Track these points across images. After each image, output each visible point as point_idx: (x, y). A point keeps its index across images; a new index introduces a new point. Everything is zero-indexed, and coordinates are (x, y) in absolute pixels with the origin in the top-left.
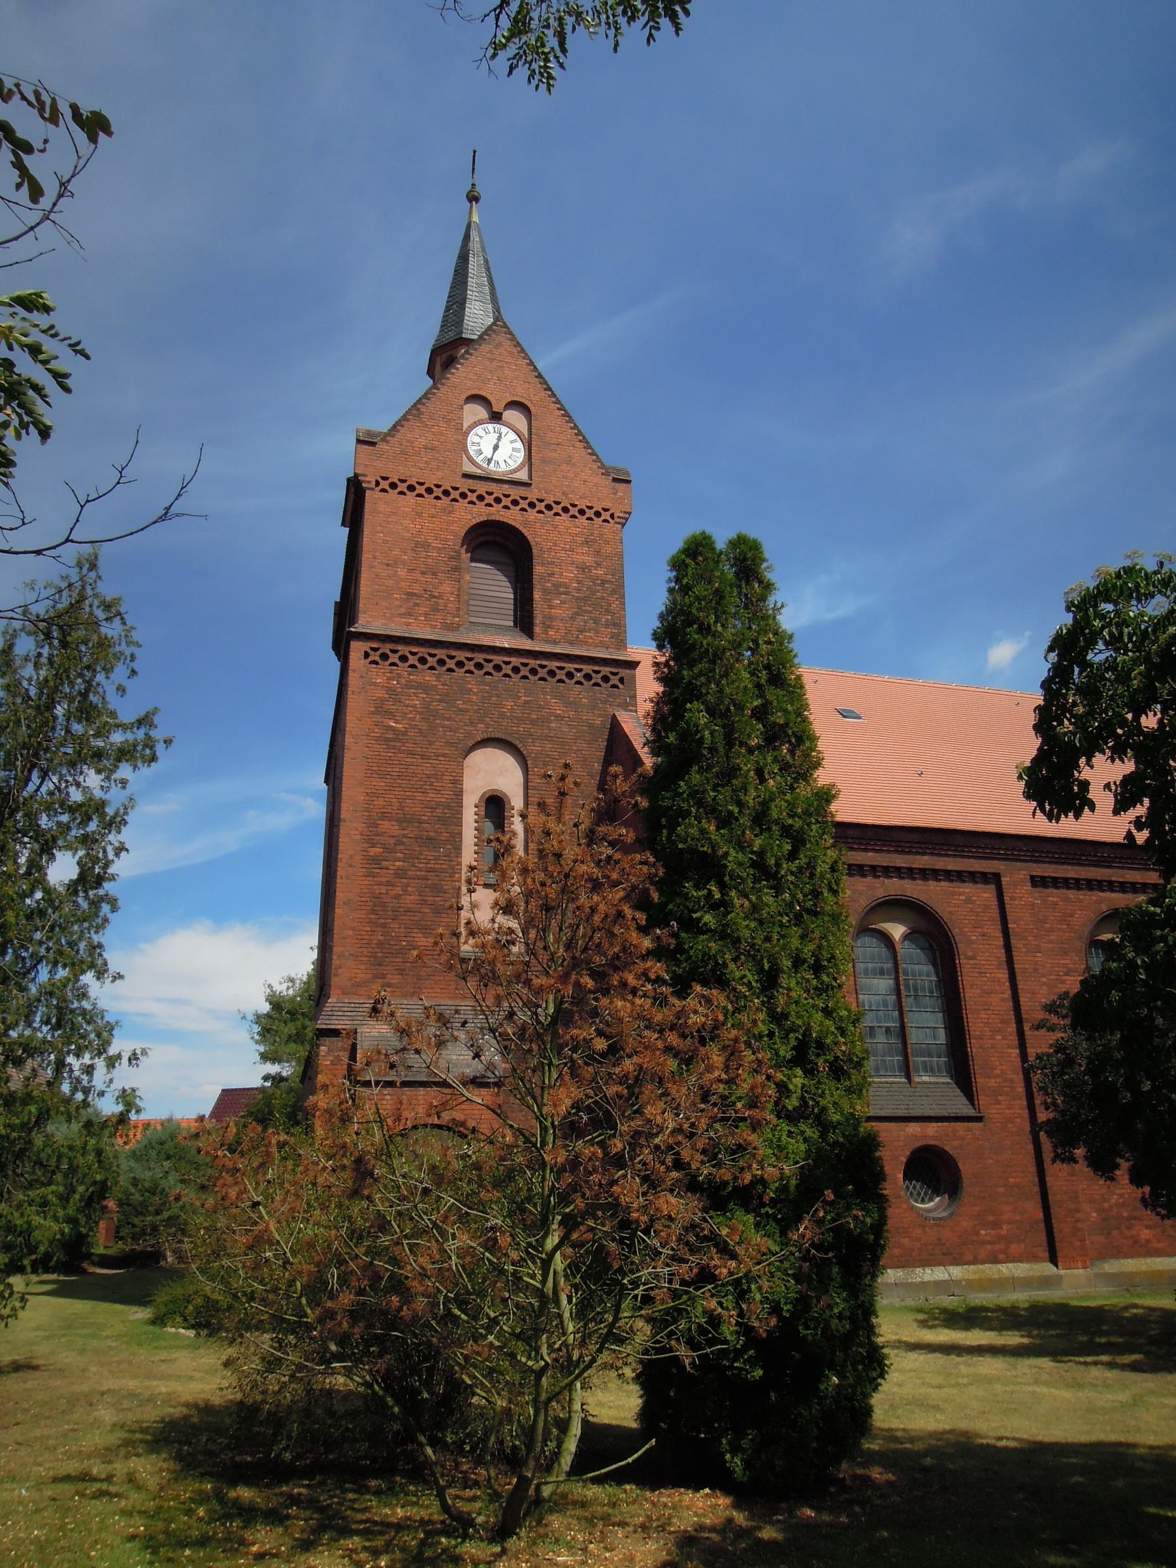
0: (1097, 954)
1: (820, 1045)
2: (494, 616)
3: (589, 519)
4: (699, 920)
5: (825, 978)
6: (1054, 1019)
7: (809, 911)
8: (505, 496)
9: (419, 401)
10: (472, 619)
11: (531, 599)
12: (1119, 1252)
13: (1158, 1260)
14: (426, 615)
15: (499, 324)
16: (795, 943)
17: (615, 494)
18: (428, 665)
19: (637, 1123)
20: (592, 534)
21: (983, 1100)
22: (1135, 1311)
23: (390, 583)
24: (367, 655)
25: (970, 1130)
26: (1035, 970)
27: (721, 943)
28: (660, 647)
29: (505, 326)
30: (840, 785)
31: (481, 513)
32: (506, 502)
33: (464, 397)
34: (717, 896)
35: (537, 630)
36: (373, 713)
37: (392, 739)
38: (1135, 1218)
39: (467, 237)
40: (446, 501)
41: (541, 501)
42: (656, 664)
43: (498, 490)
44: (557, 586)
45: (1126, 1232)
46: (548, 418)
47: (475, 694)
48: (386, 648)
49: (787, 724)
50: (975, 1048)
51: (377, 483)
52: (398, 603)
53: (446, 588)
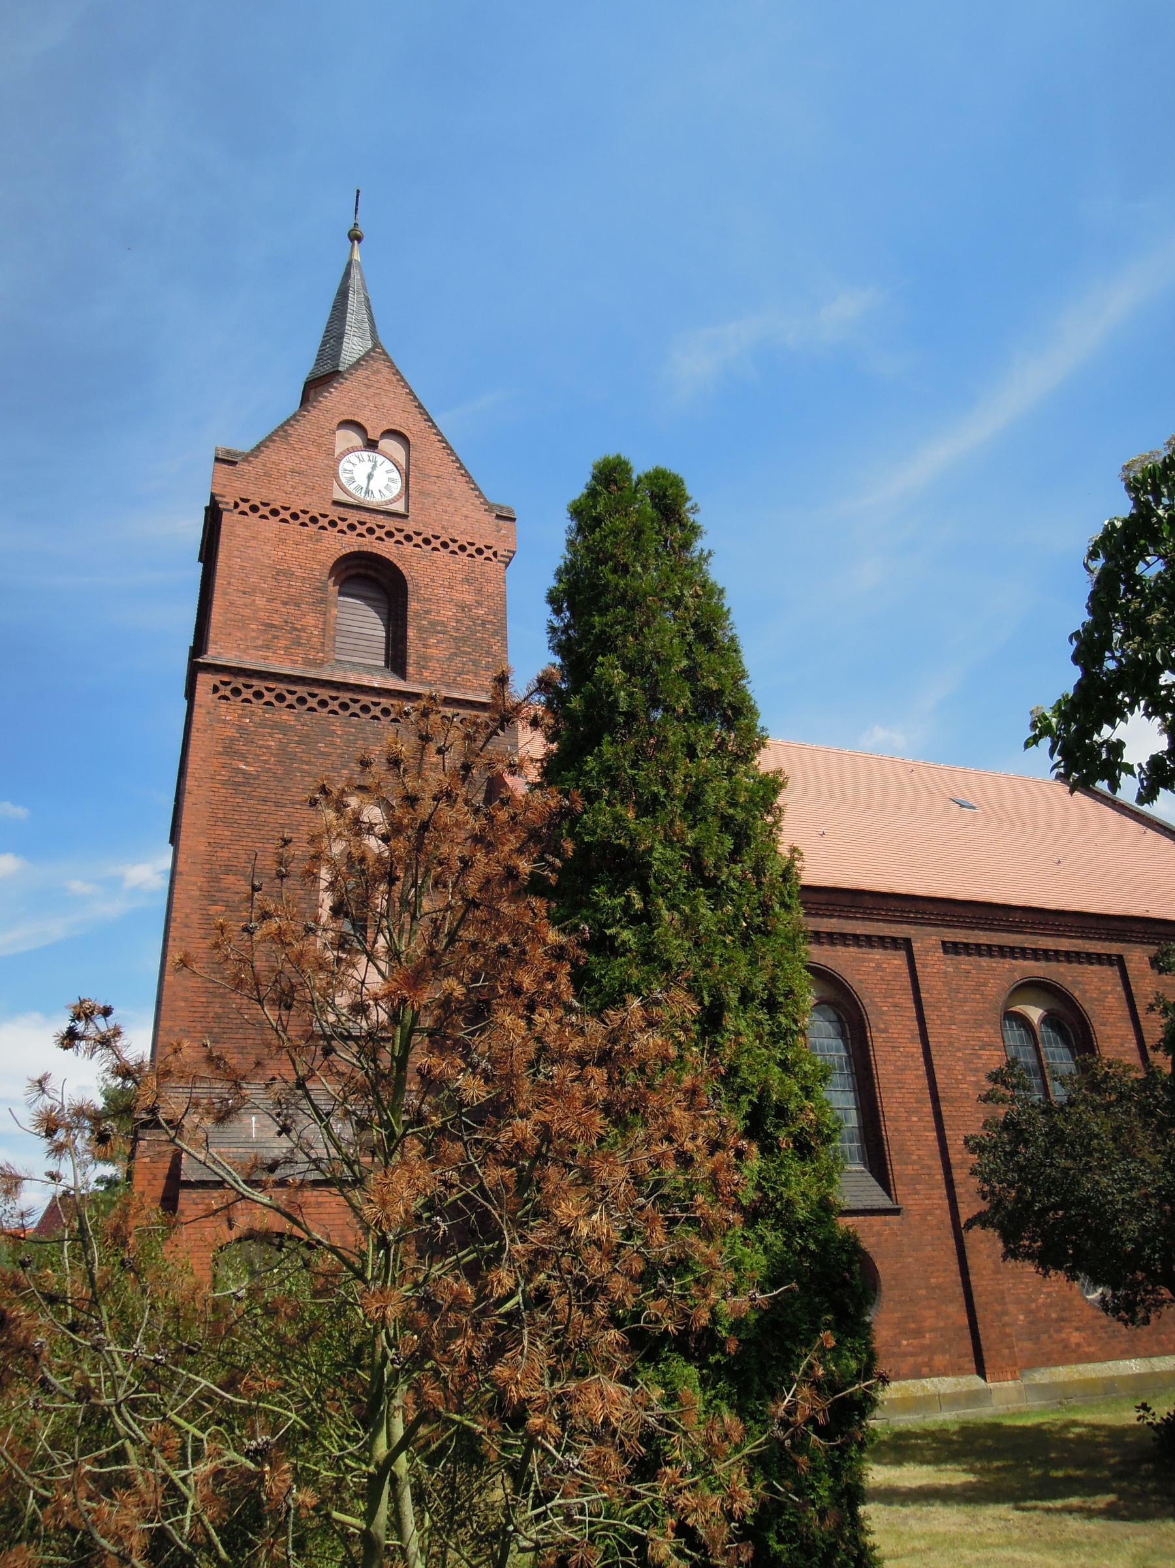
0: (1011, 1027)
1: (781, 1112)
2: (366, 655)
3: (471, 556)
4: (614, 938)
5: (782, 1019)
6: (1002, 1090)
7: (758, 930)
8: (379, 526)
9: (287, 423)
10: (338, 657)
11: (404, 637)
12: (1049, 1360)
13: (1090, 1366)
14: (286, 648)
15: (376, 352)
16: (744, 972)
17: (499, 531)
18: (286, 703)
19: (539, 1234)
20: (473, 572)
21: (900, 1189)
22: (1077, 1430)
23: (247, 612)
24: (216, 689)
25: (886, 1224)
26: (951, 1044)
27: (646, 968)
28: (557, 611)
29: (384, 353)
30: (787, 771)
31: (351, 543)
32: (380, 533)
33: (337, 421)
34: (639, 905)
35: (411, 670)
36: (220, 753)
37: (241, 784)
38: (1063, 1320)
39: (347, 274)
40: (313, 528)
41: (418, 534)
42: (553, 630)
43: (371, 520)
44: (433, 624)
45: (1055, 1336)
46: (428, 451)
47: (339, 736)
48: (238, 682)
49: (720, 692)
50: (891, 1130)
51: (236, 505)
52: (254, 634)
53: (310, 620)
